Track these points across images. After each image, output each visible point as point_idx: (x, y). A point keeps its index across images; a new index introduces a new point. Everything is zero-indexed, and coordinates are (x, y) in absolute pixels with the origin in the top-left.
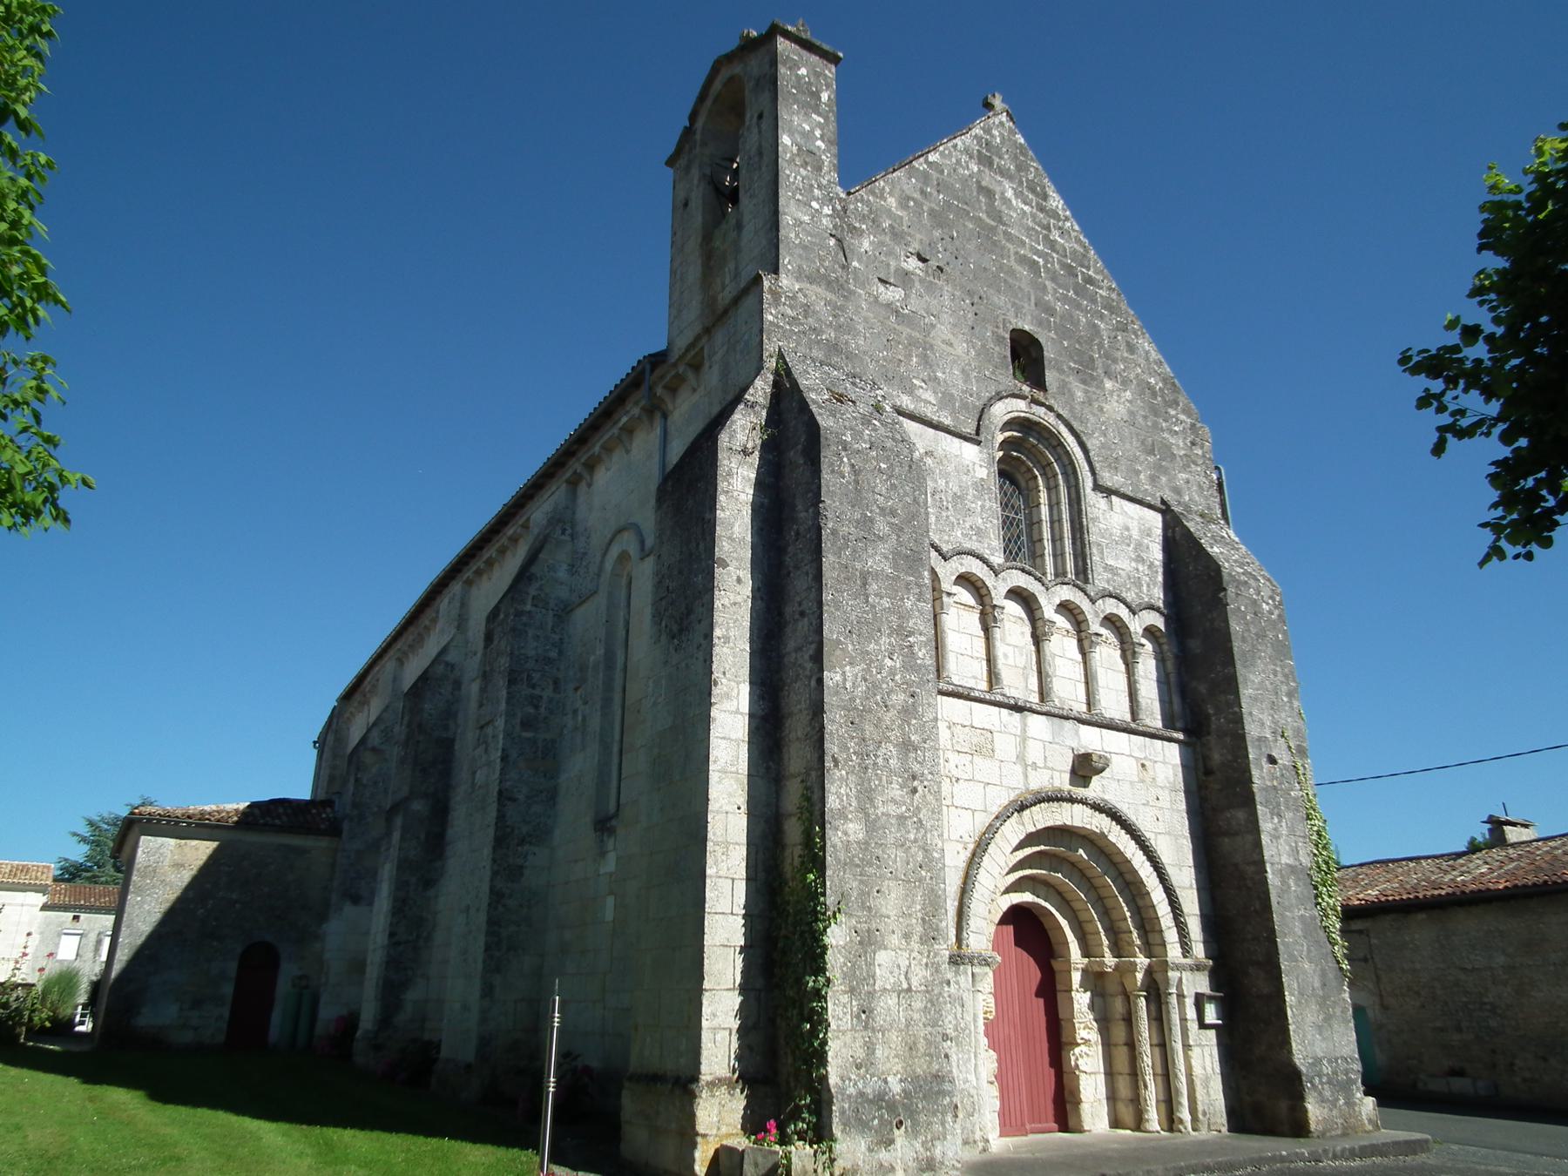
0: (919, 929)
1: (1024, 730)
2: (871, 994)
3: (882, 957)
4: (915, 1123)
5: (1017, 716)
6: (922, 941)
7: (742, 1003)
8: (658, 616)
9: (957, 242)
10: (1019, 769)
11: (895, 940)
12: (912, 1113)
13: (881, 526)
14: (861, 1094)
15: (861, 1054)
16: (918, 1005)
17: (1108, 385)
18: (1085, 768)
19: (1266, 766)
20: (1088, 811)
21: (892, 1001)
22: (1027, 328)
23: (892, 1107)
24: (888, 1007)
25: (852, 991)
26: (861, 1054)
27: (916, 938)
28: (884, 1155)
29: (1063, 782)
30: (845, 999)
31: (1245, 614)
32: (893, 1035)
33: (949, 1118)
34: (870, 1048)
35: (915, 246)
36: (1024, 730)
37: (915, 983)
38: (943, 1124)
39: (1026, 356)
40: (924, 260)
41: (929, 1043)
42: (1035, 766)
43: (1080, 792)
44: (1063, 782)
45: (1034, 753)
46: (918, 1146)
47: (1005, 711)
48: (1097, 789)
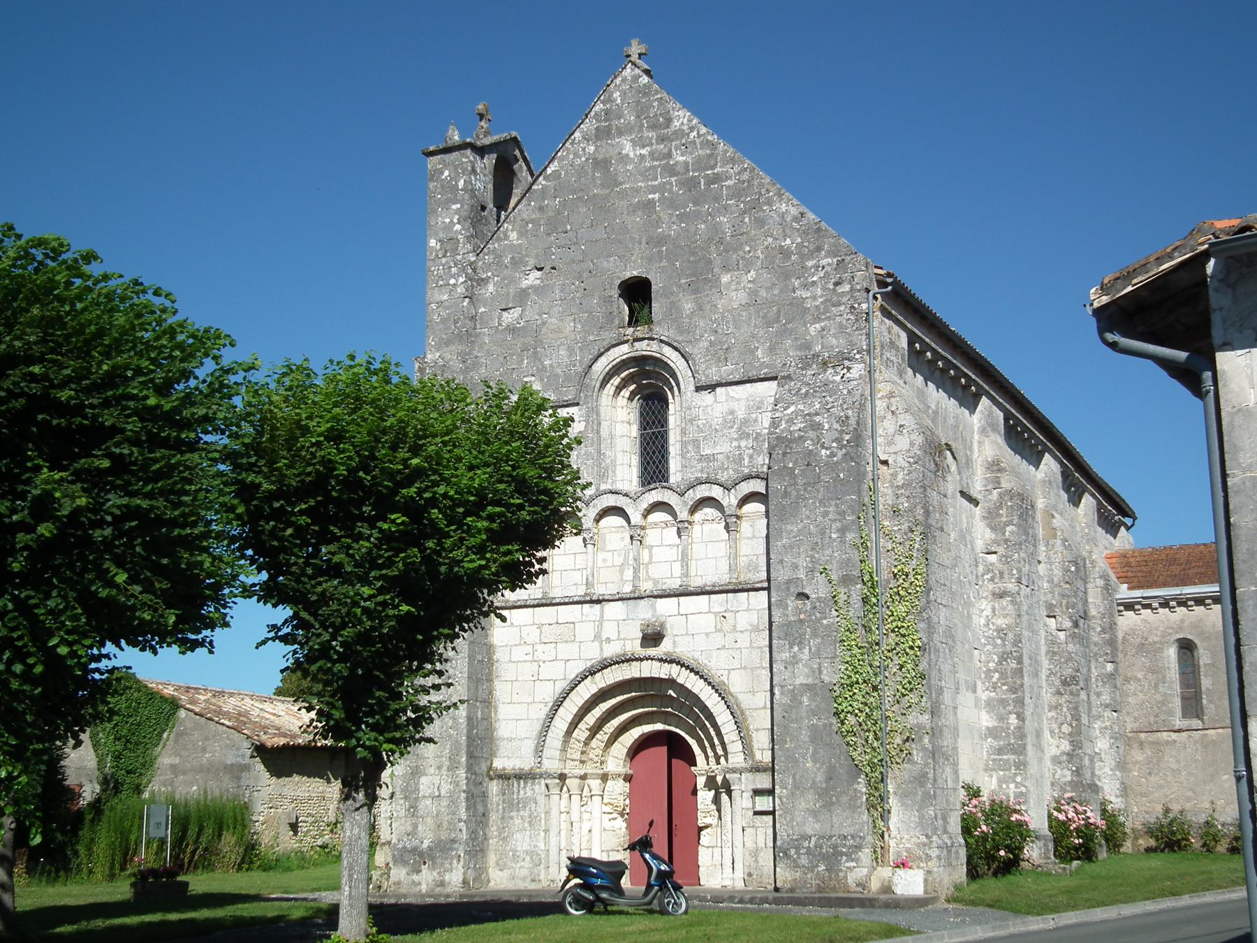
0: (447, 763)
1: (602, 616)
2: (417, 799)
3: (424, 780)
4: (434, 863)
5: (597, 607)
6: (449, 769)
7: (299, 773)
8: (53, 880)
10: (596, 644)
11: (432, 770)
12: (433, 858)
14: (404, 847)
15: (410, 829)
16: (444, 803)
17: (725, 279)
18: (653, 638)
19: (792, 603)
20: (657, 664)
21: (429, 802)
22: (635, 273)
23: (421, 854)
24: (426, 805)
25: (406, 798)
26: (410, 829)
28: (415, 877)
29: (635, 647)
30: (402, 802)
31: (793, 469)
32: (429, 820)
33: (455, 862)
34: (415, 826)
35: (532, 262)
36: (602, 616)
37: (443, 792)
38: (451, 864)
39: (637, 293)
40: (540, 269)
41: (450, 823)
42: (608, 640)
43: (652, 652)
44: (635, 647)
45: (609, 630)
46: (435, 874)
47: (586, 606)
48: (665, 647)
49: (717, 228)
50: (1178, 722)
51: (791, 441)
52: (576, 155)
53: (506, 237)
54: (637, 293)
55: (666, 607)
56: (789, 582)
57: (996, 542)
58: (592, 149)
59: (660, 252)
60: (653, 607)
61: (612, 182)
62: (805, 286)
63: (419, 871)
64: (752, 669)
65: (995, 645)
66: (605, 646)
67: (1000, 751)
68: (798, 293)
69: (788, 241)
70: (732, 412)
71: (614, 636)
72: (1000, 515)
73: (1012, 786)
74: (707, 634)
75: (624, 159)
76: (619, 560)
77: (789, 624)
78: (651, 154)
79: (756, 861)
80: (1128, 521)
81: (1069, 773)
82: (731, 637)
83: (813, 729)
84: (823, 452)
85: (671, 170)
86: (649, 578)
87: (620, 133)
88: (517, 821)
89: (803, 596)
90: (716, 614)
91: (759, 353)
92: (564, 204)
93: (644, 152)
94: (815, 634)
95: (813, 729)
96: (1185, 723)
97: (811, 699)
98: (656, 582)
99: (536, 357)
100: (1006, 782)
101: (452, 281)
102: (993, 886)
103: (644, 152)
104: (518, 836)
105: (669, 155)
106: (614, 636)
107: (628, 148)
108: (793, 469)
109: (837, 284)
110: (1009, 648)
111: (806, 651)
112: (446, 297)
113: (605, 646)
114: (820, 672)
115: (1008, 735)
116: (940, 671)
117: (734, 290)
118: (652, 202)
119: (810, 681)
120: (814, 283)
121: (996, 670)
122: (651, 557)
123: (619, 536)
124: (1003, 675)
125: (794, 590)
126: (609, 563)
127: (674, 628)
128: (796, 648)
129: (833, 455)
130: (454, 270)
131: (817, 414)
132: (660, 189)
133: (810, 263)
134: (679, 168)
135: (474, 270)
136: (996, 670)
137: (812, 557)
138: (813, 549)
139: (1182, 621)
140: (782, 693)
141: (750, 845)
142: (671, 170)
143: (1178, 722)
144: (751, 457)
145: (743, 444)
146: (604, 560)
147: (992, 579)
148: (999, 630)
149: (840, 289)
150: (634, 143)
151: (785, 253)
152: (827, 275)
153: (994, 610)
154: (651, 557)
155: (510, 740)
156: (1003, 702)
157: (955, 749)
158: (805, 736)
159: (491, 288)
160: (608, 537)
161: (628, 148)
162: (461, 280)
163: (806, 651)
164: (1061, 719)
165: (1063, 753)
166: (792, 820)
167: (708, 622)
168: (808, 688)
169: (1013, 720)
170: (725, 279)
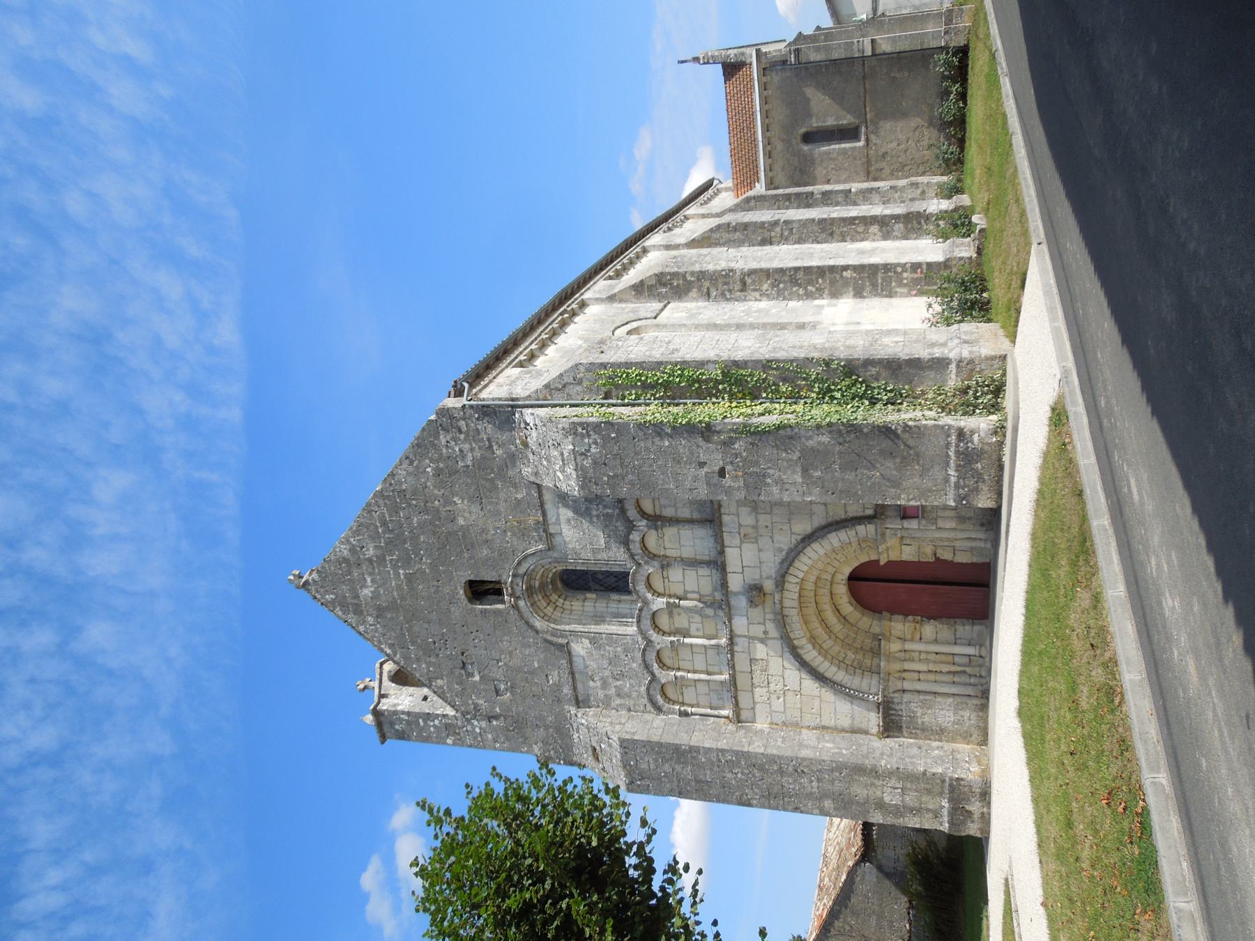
3: (887, 799)
5: (737, 640)
9: (436, 639)
13: (667, 767)
15: (930, 815)
17: (461, 522)
19: (727, 481)
26: (930, 815)
27: (876, 781)
31: (609, 476)
34: (928, 810)
39: (481, 591)
42: (765, 632)
49: (422, 525)
50: (861, 143)
51: (585, 478)
52: (376, 631)
53: (441, 687)
54: (481, 591)
55: (735, 583)
56: (708, 484)
57: (700, 289)
58: (370, 619)
59: (444, 572)
60: (736, 594)
61: (393, 606)
62: (463, 457)
63: (969, 812)
64: (791, 513)
65: (785, 289)
66: (770, 635)
67: (874, 285)
68: (469, 463)
69: (429, 470)
70: (568, 521)
71: (762, 628)
72: (678, 285)
73: (905, 275)
74: (760, 550)
75: (376, 596)
76: (697, 618)
77: (746, 486)
78: (370, 574)
79: (969, 519)
80: (715, 182)
81: (897, 226)
82: (762, 531)
83: (843, 468)
84: (593, 450)
85: (381, 560)
86: (712, 595)
87: (357, 597)
88: (926, 719)
89: (722, 473)
90: (742, 542)
91: (519, 496)
92: (413, 643)
93: (369, 580)
94: (757, 464)
95: (843, 468)
96: (863, 137)
97: (816, 469)
98: (715, 589)
99: (533, 672)
100: (902, 279)
101: (478, 730)
102: (997, 292)
103: (369, 580)
104: (940, 720)
105: (370, 560)
106: (762, 628)
107: (367, 592)
108: (609, 476)
109: (460, 432)
110: (787, 278)
111: (771, 471)
112: (490, 736)
113: (770, 635)
114: (791, 460)
115: (860, 278)
116: (794, 347)
117: (467, 513)
118: (405, 575)
119: (799, 469)
120: (461, 451)
121: (806, 289)
122: (693, 592)
123: (676, 617)
124: (810, 282)
125: (716, 479)
126: (700, 626)
127: (752, 576)
128: (769, 480)
129: (596, 443)
130: (469, 728)
131: (562, 454)
132: (395, 567)
133: (444, 451)
134: (379, 552)
135: (468, 713)
136: (806, 289)
137: (686, 463)
138: (679, 462)
139: (783, 140)
140: (810, 494)
141: (952, 524)
142: (381, 560)
143: (861, 143)
144: (605, 507)
145: (595, 513)
146: (698, 630)
147: (730, 291)
148: (773, 286)
149: (464, 429)
150: (364, 586)
151: (438, 473)
152: (454, 439)
153: (755, 290)
154: (693, 592)
155: (853, 718)
156: (833, 282)
157: (867, 332)
158: (849, 476)
159: (481, 702)
160: (677, 625)
161: (367, 592)
162: (476, 723)
163: (771, 471)
164: (852, 232)
165: (880, 230)
166: (930, 491)
167: (749, 551)
168: (805, 471)
169: (847, 274)
170: (461, 522)
